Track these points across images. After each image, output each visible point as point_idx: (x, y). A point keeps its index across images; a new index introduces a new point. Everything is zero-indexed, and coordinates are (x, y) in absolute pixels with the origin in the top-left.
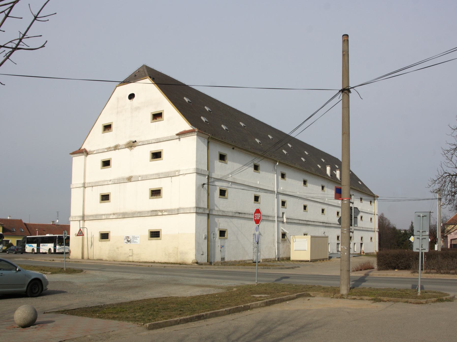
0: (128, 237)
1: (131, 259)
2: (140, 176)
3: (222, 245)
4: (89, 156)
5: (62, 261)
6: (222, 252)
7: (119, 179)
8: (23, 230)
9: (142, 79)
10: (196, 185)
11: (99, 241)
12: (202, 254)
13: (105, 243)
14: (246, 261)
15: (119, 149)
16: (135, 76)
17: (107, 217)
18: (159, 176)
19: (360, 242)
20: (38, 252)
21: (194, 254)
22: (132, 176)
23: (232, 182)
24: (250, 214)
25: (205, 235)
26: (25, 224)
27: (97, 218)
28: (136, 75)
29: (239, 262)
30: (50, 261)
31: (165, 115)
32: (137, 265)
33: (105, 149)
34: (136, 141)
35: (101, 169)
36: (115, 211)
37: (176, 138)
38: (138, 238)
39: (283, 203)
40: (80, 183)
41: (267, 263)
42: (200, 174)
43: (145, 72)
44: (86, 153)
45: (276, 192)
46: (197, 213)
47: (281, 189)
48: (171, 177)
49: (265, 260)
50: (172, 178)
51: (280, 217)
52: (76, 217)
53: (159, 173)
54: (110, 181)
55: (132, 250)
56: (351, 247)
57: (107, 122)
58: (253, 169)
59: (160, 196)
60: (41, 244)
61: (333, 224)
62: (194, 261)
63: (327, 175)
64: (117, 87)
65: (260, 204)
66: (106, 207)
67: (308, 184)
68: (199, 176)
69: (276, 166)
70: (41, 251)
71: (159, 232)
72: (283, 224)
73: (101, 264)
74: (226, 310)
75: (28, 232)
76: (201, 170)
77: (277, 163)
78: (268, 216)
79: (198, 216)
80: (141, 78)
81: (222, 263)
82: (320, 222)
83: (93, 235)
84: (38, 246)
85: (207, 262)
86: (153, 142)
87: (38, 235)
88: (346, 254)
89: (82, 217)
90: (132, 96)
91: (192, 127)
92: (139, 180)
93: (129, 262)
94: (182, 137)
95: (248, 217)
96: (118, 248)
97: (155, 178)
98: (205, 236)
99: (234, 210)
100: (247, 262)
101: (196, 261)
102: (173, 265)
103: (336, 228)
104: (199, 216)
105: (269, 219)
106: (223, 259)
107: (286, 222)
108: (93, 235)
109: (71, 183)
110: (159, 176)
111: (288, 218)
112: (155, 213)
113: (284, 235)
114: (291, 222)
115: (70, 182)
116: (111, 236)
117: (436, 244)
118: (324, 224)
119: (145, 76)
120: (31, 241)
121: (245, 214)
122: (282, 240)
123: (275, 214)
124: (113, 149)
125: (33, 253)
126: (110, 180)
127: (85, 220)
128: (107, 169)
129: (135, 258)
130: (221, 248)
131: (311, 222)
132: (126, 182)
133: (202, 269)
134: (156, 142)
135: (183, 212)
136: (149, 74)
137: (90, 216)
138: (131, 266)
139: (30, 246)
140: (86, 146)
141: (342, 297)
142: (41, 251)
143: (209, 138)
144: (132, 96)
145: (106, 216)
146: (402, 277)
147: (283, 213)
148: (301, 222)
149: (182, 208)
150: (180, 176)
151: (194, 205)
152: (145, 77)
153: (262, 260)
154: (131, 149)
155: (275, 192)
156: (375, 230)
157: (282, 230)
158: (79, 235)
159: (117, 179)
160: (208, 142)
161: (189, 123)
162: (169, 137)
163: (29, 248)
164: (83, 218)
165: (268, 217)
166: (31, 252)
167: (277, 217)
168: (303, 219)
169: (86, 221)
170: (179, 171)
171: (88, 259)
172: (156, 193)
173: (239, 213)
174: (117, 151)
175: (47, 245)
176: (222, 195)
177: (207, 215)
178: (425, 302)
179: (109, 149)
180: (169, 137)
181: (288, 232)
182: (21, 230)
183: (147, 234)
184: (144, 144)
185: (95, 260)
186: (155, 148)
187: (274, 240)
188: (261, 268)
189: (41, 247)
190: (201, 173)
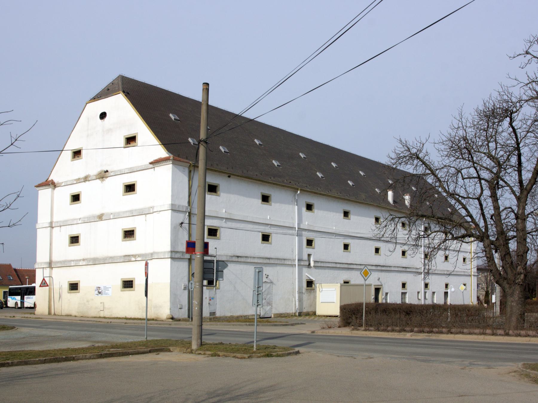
0: (99, 288)
1: (102, 314)
2: (112, 214)
3: (212, 296)
4: (57, 189)
5: (22, 317)
6: (211, 305)
7: (89, 218)
8: (12, 279)
9: (114, 94)
10: (171, 224)
11: (121, 291)
12: (180, 308)
13: (74, 296)
14: (249, 316)
15: (89, 181)
16: (108, 90)
17: (76, 264)
18: (133, 214)
19: (444, 290)
20: (22, 307)
21: (169, 308)
22: (104, 214)
23: (226, 219)
24: (254, 258)
25: (184, 284)
26: (15, 270)
27: (66, 264)
28: (110, 88)
29: (238, 317)
30: (11, 317)
31: (139, 139)
32: (96, 321)
33: (74, 181)
34: (108, 170)
35: (70, 205)
36: (86, 257)
37: (150, 167)
38: (109, 289)
39: (310, 243)
40: (46, 223)
41: (279, 319)
42: (177, 210)
43: (119, 86)
44: (53, 185)
45: (297, 229)
46: (172, 258)
47: (305, 224)
48: (145, 215)
49: (279, 315)
50: (146, 216)
51: (303, 260)
52: (42, 264)
53: (133, 210)
54: (79, 220)
55: (104, 303)
56: (427, 298)
57: (76, 147)
58: (260, 201)
59: (134, 237)
60: (25, 297)
61: (394, 267)
62: (168, 317)
63: (389, 203)
64: (88, 104)
65: (271, 244)
66: (75, 252)
67: (351, 216)
68: (176, 213)
69: (297, 195)
70: (26, 305)
71: (132, 281)
72: (309, 269)
73: (61, 321)
74: (39, 360)
75: (19, 280)
76: (179, 206)
77: (298, 192)
78: (285, 259)
79: (175, 262)
80: (113, 93)
81: (211, 319)
82: (373, 265)
83: (62, 286)
84: (22, 299)
85: (187, 317)
86: (125, 172)
87: (28, 285)
88: (196, 308)
89: (48, 264)
90: (103, 116)
91: (168, 154)
92: (111, 218)
93: (100, 317)
94: (157, 166)
95: (252, 261)
96: (88, 301)
97: (128, 216)
98: (184, 286)
99: (230, 254)
100: (250, 317)
101: (171, 317)
102: (139, 321)
103: (400, 273)
104: (176, 263)
105: (286, 263)
106: (213, 314)
107: (314, 266)
108: (62, 286)
109: (37, 222)
110: (132, 213)
111: (317, 261)
112: (127, 258)
113: (310, 283)
114: (321, 265)
115: (36, 221)
116: (81, 286)
117: (493, 295)
118: (379, 268)
119: (119, 90)
120: (13, 293)
121: (247, 258)
122: (306, 289)
123: (295, 256)
124: (83, 181)
125: (17, 307)
126: (80, 219)
127: (52, 268)
128: (76, 205)
129: (107, 314)
130: (210, 300)
131: (355, 265)
132: (97, 221)
133: (170, 326)
134: (129, 172)
135: (157, 258)
136: (123, 88)
137: (58, 262)
138: (83, 322)
139: (13, 299)
140: (54, 177)
141: (191, 352)
142: (26, 305)
143: (190, 166)
144: (103, 116)
145: (75, 262)
146: (341, 335)
147: (309, 255)
148: (338, 266)
149: (156, 253)
150: (154, 213)
151: (169, 249)
152: (118, 91)
153: (274, 315)
154: (103, 181)
155: (295, 228)
156: (471, 273)
157: (307, 277)
158: (42, 285)
159: (87, 217)
160: (190, 172)
161: (165, 149)
162: (143, 166)
163: (12, 301)
164: (50, 265)
165: (283, 261)
166: (14, 306)
167: (298, 260)
168: (343, 262)
169: (53, 268)
170: (153, 207)
171: (55, 314)
172: (129, 234)
173: (238, 257)
174: (87, 182)
175: (32, 298)
176: (211, 236)
177: (187, 260)
178: (247, 357)
179: (78, 181)
180: (143, 166)
181: (314, 280)
182: (10, 278)
183: (120, 284)
184: (117, 174)
185: (63, 316)
186: (129, 179)
187: (294, 289)
188: (246, 324)
189: (25, 299)
190: (177, 210)
